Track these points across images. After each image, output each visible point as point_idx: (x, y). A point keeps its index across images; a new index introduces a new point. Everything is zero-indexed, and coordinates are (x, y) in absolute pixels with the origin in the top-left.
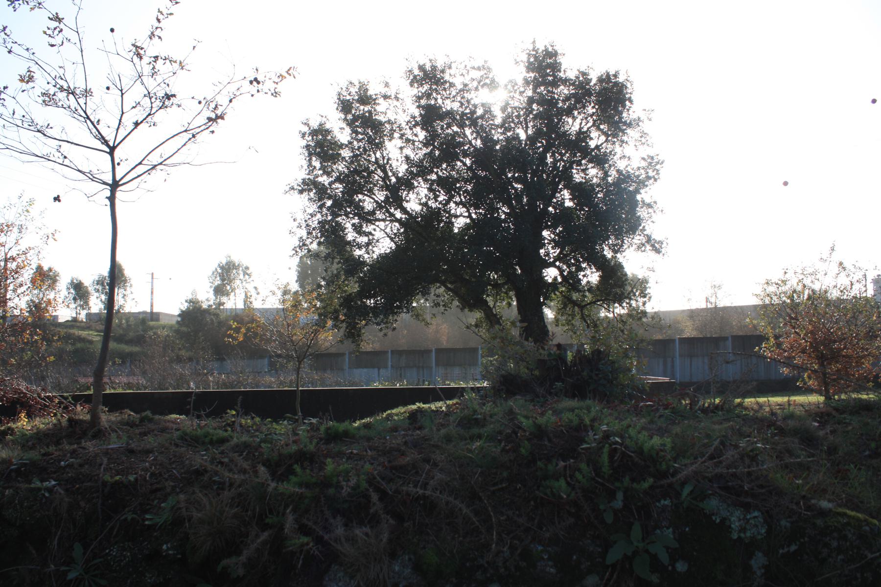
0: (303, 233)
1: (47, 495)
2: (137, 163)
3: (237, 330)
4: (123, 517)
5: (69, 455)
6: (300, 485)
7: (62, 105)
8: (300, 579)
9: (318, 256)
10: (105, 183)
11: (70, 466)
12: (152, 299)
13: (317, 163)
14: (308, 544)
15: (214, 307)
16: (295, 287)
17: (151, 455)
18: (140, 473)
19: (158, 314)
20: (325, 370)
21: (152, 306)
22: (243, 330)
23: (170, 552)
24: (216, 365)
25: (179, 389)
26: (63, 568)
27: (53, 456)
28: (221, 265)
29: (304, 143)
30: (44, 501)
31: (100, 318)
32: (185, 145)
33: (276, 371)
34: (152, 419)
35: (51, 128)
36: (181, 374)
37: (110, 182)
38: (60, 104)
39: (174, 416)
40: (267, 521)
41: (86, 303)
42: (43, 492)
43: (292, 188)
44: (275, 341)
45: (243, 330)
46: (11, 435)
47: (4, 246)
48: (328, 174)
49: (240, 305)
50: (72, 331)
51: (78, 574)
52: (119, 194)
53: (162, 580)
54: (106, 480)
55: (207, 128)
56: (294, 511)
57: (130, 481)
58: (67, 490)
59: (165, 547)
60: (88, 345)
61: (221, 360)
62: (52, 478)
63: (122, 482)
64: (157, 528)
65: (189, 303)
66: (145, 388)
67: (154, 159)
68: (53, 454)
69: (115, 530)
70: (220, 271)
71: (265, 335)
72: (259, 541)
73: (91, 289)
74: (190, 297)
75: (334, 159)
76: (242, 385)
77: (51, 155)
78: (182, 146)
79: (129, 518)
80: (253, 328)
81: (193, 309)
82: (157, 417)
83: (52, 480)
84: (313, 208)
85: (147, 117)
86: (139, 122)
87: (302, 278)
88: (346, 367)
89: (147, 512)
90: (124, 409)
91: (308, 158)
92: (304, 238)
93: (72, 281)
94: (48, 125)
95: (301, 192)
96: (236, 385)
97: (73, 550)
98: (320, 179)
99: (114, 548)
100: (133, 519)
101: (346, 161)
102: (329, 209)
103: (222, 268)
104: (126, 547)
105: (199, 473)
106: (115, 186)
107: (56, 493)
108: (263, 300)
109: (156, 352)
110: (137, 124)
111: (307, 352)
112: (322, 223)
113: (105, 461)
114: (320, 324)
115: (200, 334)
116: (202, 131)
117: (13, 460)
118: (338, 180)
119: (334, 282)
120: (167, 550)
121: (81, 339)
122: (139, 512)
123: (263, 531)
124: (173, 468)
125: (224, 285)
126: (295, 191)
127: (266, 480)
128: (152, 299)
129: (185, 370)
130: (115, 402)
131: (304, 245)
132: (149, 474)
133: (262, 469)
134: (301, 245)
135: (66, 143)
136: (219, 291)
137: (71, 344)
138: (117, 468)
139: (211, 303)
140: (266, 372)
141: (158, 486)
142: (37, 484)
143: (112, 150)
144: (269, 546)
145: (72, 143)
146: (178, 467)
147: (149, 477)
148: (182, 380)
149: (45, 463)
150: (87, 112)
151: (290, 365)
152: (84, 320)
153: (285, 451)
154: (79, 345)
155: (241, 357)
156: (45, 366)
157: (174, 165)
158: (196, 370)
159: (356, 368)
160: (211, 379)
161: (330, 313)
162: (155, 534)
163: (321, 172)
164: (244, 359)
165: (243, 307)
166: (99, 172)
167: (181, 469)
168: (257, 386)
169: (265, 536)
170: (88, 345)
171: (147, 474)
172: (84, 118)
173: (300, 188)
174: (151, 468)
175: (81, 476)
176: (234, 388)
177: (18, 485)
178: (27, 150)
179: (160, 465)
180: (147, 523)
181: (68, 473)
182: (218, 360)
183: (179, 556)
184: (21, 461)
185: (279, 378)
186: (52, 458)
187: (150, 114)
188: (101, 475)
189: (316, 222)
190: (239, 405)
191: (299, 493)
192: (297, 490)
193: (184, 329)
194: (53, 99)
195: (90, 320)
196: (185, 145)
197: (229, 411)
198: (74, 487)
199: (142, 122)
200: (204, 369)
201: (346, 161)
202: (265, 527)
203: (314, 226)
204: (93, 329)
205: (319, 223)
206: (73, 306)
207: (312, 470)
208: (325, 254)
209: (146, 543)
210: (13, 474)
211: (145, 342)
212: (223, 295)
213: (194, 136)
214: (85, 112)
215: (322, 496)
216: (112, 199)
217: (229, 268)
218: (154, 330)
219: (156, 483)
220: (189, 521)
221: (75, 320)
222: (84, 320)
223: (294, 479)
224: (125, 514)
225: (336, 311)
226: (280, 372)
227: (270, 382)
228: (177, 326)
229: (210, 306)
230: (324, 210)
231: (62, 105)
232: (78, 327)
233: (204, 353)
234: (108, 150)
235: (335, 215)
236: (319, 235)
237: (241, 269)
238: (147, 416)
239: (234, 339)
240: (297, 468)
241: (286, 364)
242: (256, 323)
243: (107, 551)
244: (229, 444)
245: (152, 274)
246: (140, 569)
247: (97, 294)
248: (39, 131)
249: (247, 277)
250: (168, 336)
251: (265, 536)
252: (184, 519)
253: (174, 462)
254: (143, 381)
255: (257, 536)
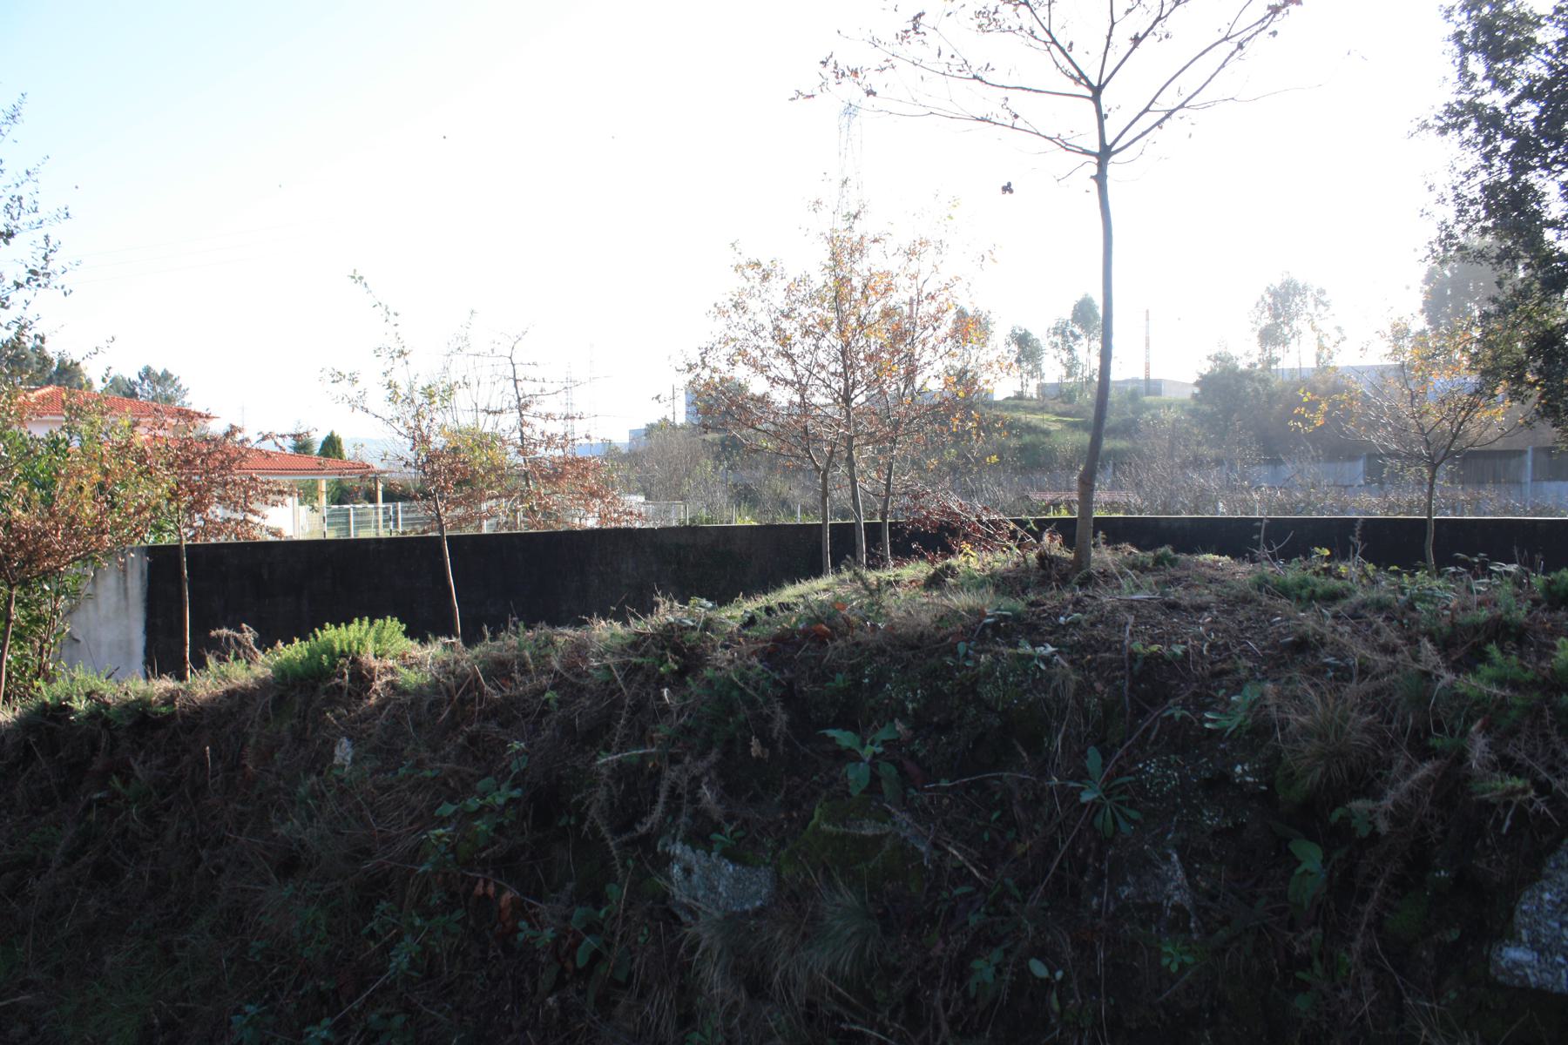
0: (1450, 212)
1: (1042, 666)
2: (1141, 111)
3: (1312, 406)
4: (1167, 714)
5: (1071, 607)
6: (1501, 682)
7: (1010, 27)
8: (1494, 857)
9: (1483, 256)
10: (1085, 152)
11: (1076, 624)
12: (1147, 356)
13: (1477, 65)
14: (1524, 791)
15: (1259, 366)
16: (1420, 324)
17: (1206, 614)
18: (1190, 642)
19: (1158, 383)
20: (1481, 483)
21: (1147, 368)
22: (1324, 406)
23: (1249, 779)
24: (1266, 471)
25: (1198, 514)
26: (1072, 784)
27: (1045, 607)
28: (1272, 289)
29: (1451, 29)
30: (1038, 676)
31: (1061, 392)
32: (1223, 66)
33: (1382, 483)
34: (1176, 559)
35: (993, 69)
36: (1203, 490)
37: (1096, 149)
38: (1005, 27)
39: (1210, 557)
40: (1432, 742)
41: (1037, 367)
42: (1036, 662)
43: (1425, 126)
44: (1384, 426)
45: (1324, 406)
46: (952, 577)
47: (916, 278)
48: (1503, 84)
49: (1309, 363)
50: (1016, 415)
51: (1095, 796)
52: (1111, 169)
53: (1230, 824)
54: (1135, 650)
55: (1264, 28)
56: (1487, 729)
57: (1175, 654)
58: (1072, 662)
59: (1239, 769)
60: (1042, 438)
61: (1275, 462)
62: (1049, 642)
63: (1162, 656)
64: (1226, 735)
65: (1214, 361)
66: (1141, 511)
67: (1168, 100)
68: (1044, 605)
69: (1154, 734)
70: (1270, 300)
71: (1366, 415)
72: (1415, 776)
73: (1044, 343)
74: (1214, 351)
75: (1519, 52)
76: (1315, 507)
77: (994, 116)
78: (1219, 69)
79: (1177, 715)
80: (1343, 402)
81: (1222, 372)
82: (1183, 557)
83: (1048, 645)
84: (1474, 158)
85: (1155, 23)
86: (1140, 36)
87: (1434, 307)
88: (1527, 476)
89: (1207, 708)
90: (1120, 543)
91: (1458, 61)
92: (1450, 222)
93: (1013, 331)
94: (988, 65)
95: (1443, 131)
96: (1303, 508)
97: (1086, 757)
98: (1485, 100)
99: (1152, 762)
100: (1183, 718)
101: (1548, 52)
102: (1505, 157)
103: (1274, 294)
104: (1172, 762)
105: (1302, 645)
106: (1105, 154)
107: (1056, 665)
108: (1362, 349)
109: (1157, 449)
110: (1137, 40)
111: (1450, 446)
112: (1490, 191)
113: (1131, 619)
114: (1483, 393)
115: (1235, 415)
116: (1257, 33)
117: (986, 610)
118: (1527, 94)
119: (1516, 306)
120: (1241, 776)
121: (1030, 429)
122: (1192, 707)
123: (1422, 760)
124: (1246, 638)
125: (1278, 325)
126: (1431, 131)
127: (1435, 667)
128: (1147, 356)
129: (1212, 480)
130: (1117, 531)
131: (1450, 236)
132: (1206, 645)
133: (1427, 646)
134: (1443, 237)
135: (1021, 91)
136: (1269, 336)
137: (1015, 436)
138: (1150, 632)
139: (1254, 359)
140: (1360, 486)
141: (1224, 666)
142: (1025, 648)
143: (1097, 91)
144: (1432, 787)
145: (1030, 90)
146: (1256, 637)
147: (1208, 651)
148: (1203, 497)
149: (1035, 618)
150: (1052, 32)
151: (1410, 475)
152: (1035, 396)
153: (1461, 618)
154: (1027, 438)
155: (1313, 458)
156: (978, 472)
157: (1206, 106)
158: (1228, 482)
159: (1549, 480)
160: (1256, 497)
161: (1507, 368)
162: (1222, 746)
163: (1488, 84)
164: (1319, 461)
165: (1315, 366)
166: (1073, 134)
167: (1262, 640)
168: (1343, 511)
169: (1426, 769)
170: (1042, 438)
171: (1203, 646)
172: (1046, 42)
173: (1442, 124)
174: (1209, 635)
175: (1093, 642)
176: (1300, 513)
177: (997, 649)
178: (961, 112)
179: (1225, 631)
180: (1207, 725)
181: (1073, 635)
182: (1268, 462)
183: (1264, 788)
184: (999, 612)
185: (1386, 496)
186: (1044, 611)
187: (1159, 18)
188: (1126, 642)
189: (1479, 187)
190: (1357, 533)
191: (1499, 697)
192: (1495, 691)
193: (1206, 408)
194: (994, 20)
195: (1044, 395)
196: (1223, 66)
197: (1317, 549)
198: (1083, 658)
199: (1145, 35)
200: (1243, 480)
201: (1548, 52)
202: (1425, 753)
203: (1471, 197)
204: (1050, 410)
205: (1484, 189)
206: (1015, 372)
207: (1521, 657)
208: (1498, 251)
209: (1205, 760)
210: (988, 631)
211: (1138, 431)
212: (1276, 344)
213: (1240, 46)
214: (1049, 33)
215: (1546, 707)
216: (1101, 178)
217: (1288, 294)
218: (1152, 411)
219: (1220, 661)
220: (1282, 729)
221: (1020, 396)
222: (1035, 396)
223: (1485, 670)
224: (1170, 708)
225: (1520, 366)
226: (1387, 486)
227: (1368, 504)
228: (1192, 403)
229: (1252, 365)
230: (1496, 161)
231: (1010, 27)
232: (1025, 408)
233: (1244, 450)
234: (1090, 94)
235: (1519, 169)
236: (1483, 214)
237: (1309, 293)
238: (1165, 555)
239: (1306, 422)
240: (1493, 649)
241: (1402, 469)
242: (1349, 393)
243: (1140, 766)
244: (1345, 602)
245: (1147, 311)
246: (1195, 801)
247: (1055, 351)
248: (975, 77)
249: (1321, 307)
250: (1177, 420)
251: (1426, 769)
252: (1274, 726)
253: (1247, 629)
254: (1135, 499)
255: (1409, 769)
